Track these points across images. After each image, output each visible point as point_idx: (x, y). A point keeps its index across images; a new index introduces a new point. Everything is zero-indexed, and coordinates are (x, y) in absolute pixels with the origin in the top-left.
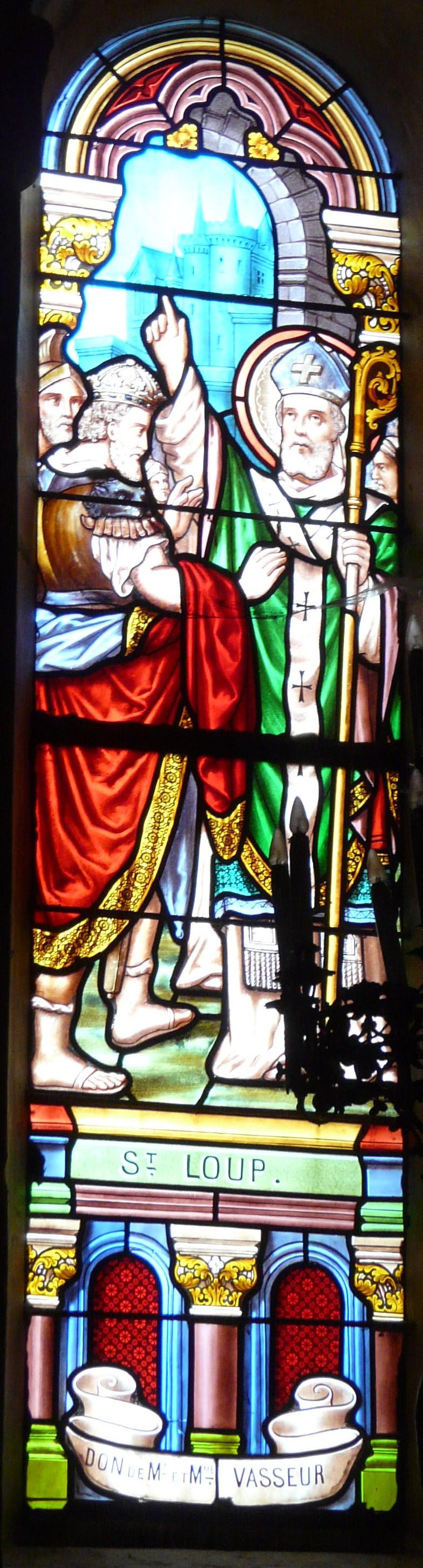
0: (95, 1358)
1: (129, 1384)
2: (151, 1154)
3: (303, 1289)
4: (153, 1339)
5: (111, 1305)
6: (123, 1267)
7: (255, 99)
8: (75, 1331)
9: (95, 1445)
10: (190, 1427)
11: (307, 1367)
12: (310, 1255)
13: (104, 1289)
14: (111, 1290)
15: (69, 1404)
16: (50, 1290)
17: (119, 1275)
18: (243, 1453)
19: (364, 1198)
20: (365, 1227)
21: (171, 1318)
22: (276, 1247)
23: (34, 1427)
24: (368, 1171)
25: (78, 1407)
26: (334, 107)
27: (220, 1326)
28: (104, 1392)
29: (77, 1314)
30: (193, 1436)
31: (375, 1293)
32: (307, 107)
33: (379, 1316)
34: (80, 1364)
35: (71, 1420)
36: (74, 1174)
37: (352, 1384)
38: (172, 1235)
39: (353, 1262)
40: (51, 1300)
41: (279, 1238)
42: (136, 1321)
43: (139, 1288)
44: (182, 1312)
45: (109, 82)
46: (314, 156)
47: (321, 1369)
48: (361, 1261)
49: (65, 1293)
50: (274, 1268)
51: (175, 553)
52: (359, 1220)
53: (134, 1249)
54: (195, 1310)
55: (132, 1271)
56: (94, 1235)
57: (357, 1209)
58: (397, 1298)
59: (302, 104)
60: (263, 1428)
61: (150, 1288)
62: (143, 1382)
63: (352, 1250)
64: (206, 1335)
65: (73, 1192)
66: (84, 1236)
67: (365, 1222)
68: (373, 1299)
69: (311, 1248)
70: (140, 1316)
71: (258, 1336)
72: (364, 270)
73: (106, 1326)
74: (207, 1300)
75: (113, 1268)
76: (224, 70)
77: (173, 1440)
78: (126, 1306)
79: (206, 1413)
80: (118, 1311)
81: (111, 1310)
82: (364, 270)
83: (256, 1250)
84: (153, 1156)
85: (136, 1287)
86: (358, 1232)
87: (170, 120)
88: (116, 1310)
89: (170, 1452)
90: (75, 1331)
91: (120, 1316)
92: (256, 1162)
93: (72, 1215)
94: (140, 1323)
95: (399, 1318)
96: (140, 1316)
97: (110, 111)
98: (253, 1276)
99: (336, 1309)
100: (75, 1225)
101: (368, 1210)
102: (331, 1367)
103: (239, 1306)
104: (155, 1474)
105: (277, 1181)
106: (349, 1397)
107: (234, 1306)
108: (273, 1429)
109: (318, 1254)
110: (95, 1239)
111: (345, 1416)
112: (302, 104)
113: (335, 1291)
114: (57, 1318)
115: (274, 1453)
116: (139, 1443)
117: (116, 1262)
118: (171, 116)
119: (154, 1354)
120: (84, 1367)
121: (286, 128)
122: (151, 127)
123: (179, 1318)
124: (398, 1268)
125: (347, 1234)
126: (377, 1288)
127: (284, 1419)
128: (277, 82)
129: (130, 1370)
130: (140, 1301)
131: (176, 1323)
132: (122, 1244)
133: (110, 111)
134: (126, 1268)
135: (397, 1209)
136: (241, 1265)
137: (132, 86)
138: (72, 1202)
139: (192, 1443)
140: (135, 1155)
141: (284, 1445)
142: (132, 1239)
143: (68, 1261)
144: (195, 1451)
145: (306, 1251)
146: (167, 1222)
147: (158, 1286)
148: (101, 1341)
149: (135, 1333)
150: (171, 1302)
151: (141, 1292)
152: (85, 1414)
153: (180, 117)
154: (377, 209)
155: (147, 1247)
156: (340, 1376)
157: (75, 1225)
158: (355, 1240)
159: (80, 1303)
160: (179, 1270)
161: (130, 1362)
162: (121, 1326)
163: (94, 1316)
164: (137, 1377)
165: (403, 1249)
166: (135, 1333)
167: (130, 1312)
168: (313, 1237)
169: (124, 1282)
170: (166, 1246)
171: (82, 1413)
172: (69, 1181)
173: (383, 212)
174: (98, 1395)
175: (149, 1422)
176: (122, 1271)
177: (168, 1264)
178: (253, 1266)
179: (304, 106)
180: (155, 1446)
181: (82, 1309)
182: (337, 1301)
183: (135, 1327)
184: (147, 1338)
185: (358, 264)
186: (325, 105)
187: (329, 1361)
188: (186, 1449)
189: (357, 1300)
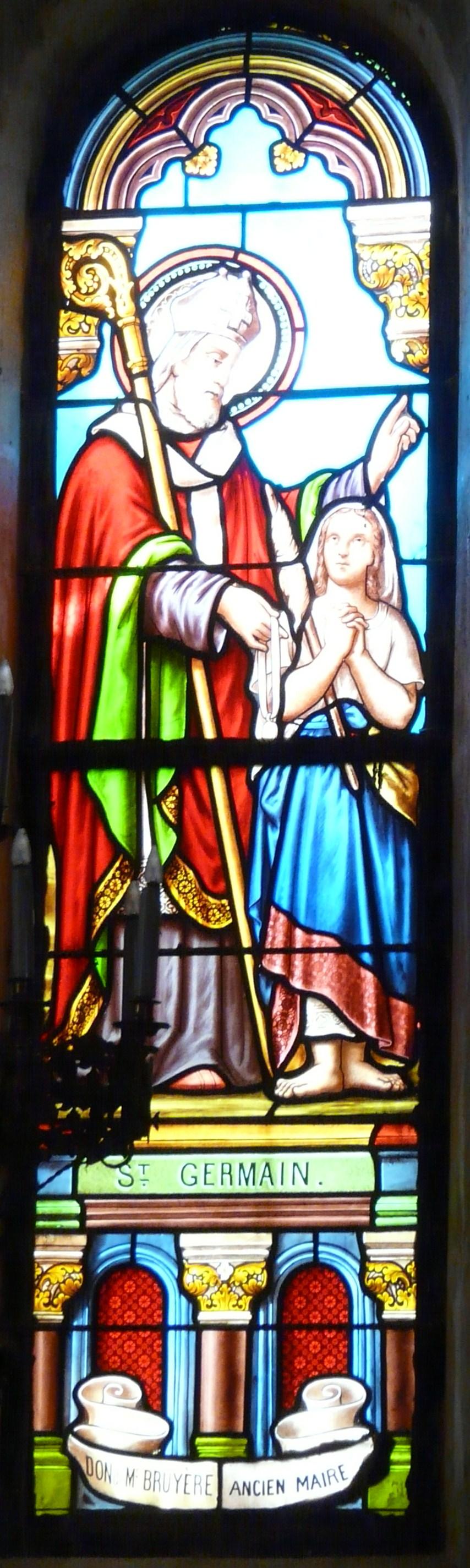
0: (98, 1368)
1: (136, 1392)
2: (144, 1166)
3: (124, 1292)
4: (158, 1346)
5: (300, 1318)
6: (312, 1278)
7: (278, 110)
8: (78, 1343)
9: (95, 1454)
10: (195, 1431)
11: (315, 1369)
12: (320, 1256)
13: (293, 1302)
14: (299, 1303)
15: (73, 1414)
16: (55, 1306)
17: (122, 1287)
18: (250, 1457)
19: (378, 1193)
20: (379, 1222)
21: (178, 1328)
22: (286, 1248)
23: (37, 1439)
24: (383, 1165)
25: (83, 1416)
26: (361, 103)
27: (45, 1332)
28: (109, 1399)
29: (81, 1328)
30: (199, 1440)
31: (386, 1290)
32: (331, 104)
33: (388, 1314)
34: (85, 1375)
35: (76, 1429)
36: (81, 1189)
37: (362, 1382)
38: (182, 1244)
39: (364, 1260)
40: (57, 1316)
41: (289, 1239)
42: (296, 1331)
43: (328, 1297)
44: (188, 1322)
45: (130, 117)
46: (339, 153)
47: (330, 1370)
48: (372, 1259)
49: (70, 1309)
50: (284, 1270)
51: (142, 577)
52: (373, 1214)
53: (140, 1259)
54: (203, 1317)
55: (321, 1282)
56: (282, 1249)
57: (372, 1204)
58: (409, 1295)
59: (325, 103)
60: (269, 1432)
61: (340, 1297)
62: (148, 1390)
63: (363, 1247)
64: (211, 1340)
65: (84, 1208)
66: (90, 1251)
67: (379, 1216)
68: (384, 1296)
69: (321, 1248)
70: (330, 1327)
71: (265, 1341)
72: (391, 260)
73: (295, 1337)
74: (215, 1306)
75: (116, 1281)
76: (248, 86)
77: (178, 1446)
78: (129, 1317)
79: (210, 1420)
80: (307, 1323)
81: (330, 1322)
82: (391, 260)
83: (267, 1253)
84: (146, 1167)
85: (325, 1297)
86: (372, 1227)
87: (189, 145)
88: (305, 1321)
89: (174, 1457)
90: (78, 1343)
91: (310, 1327)
92: (225, 1166)
93: (82, 1230)
94: (300, 1333)
95: (412, 1315)
96: (330, 1327)
97: (132, 144)
98: (263, 1277)
99: (345, 1308)
100: (82, 1240)
101: (383, 1204)
102: (340, 1367)
103: (249, 1310)
104: (151, 1482)
105: (320, 1183)
106: (359, 1394)
107: (244, 1310)
108: (278, 1431)
109: (327, 1254)
110: (288, 1249)
111: (356, 1411)
112: (325, 103)
113: (158, 1290)
114: (61, 1333)
115: (280, 1455)
116: (133, 1449)
117: (119, 1274)
118: (191, 140)
119: (159, 1360)
120: (89, 1377)
121: (308, 130)
122: (168, 156)
123: (187, 1328)
124: (410, 1264)
125: (359, 1230)
126: (388, 1286)
127: (290, 1420)
128: (299, 87)
129: (136, 1379)
130: (330, 1310)
131: (184, 1333)
132: (311, 1255)
133: (132, 144)
134: (315, 1279)
135: (411, 1203)
136: (251, 1270)
137: (156, 116)
138: (82, 1217)
139: (199, 1448)
140: (195, 1167)
141: (287, 1445)
142: (138, 1250)
143: (73, 1275)
144: (201, 1456)
145: (315, 1251)
146: (176, 1231)
147: (348, 1294)
148: (105, 1352)
149: (325, 1342)
150: (177, 1311)
151: (330, 1302)
152: (90, 1422)
153: (201, 141)
154: (404, 195)
155: (156, 1259)
156: (349, 1374)
157: (82, 1240)
158: (368, 1237)
159: (84, 1319)
160: (187, 1279)
161: (135, 1371)
162: (310, 1337)
163: (97, 1331)
164: (142, 1385)
165: (418, 1245)
166: (325, 1342)
167: (320, 1322)
168: (323, 1237)
169: (127, 1293)
170: (173, 1254)
171: (87, 1423)
172: (75, 1196)
173: (412, 196)
174: (102, 1402)
175: (154, 1428)
176: (310, 1282)
177: (176, 1274)
178: (263, 1269)
179: (328, 104)
180: (157, 1450)
181: (86, 1323)
182: (346, 1302)
183: (325, 1337)
184: (151, 1346)
185: (382, 255)
186: (352, 102)
187: (338, 1362)
188: (192, 1455)
189: (367, 1298)
